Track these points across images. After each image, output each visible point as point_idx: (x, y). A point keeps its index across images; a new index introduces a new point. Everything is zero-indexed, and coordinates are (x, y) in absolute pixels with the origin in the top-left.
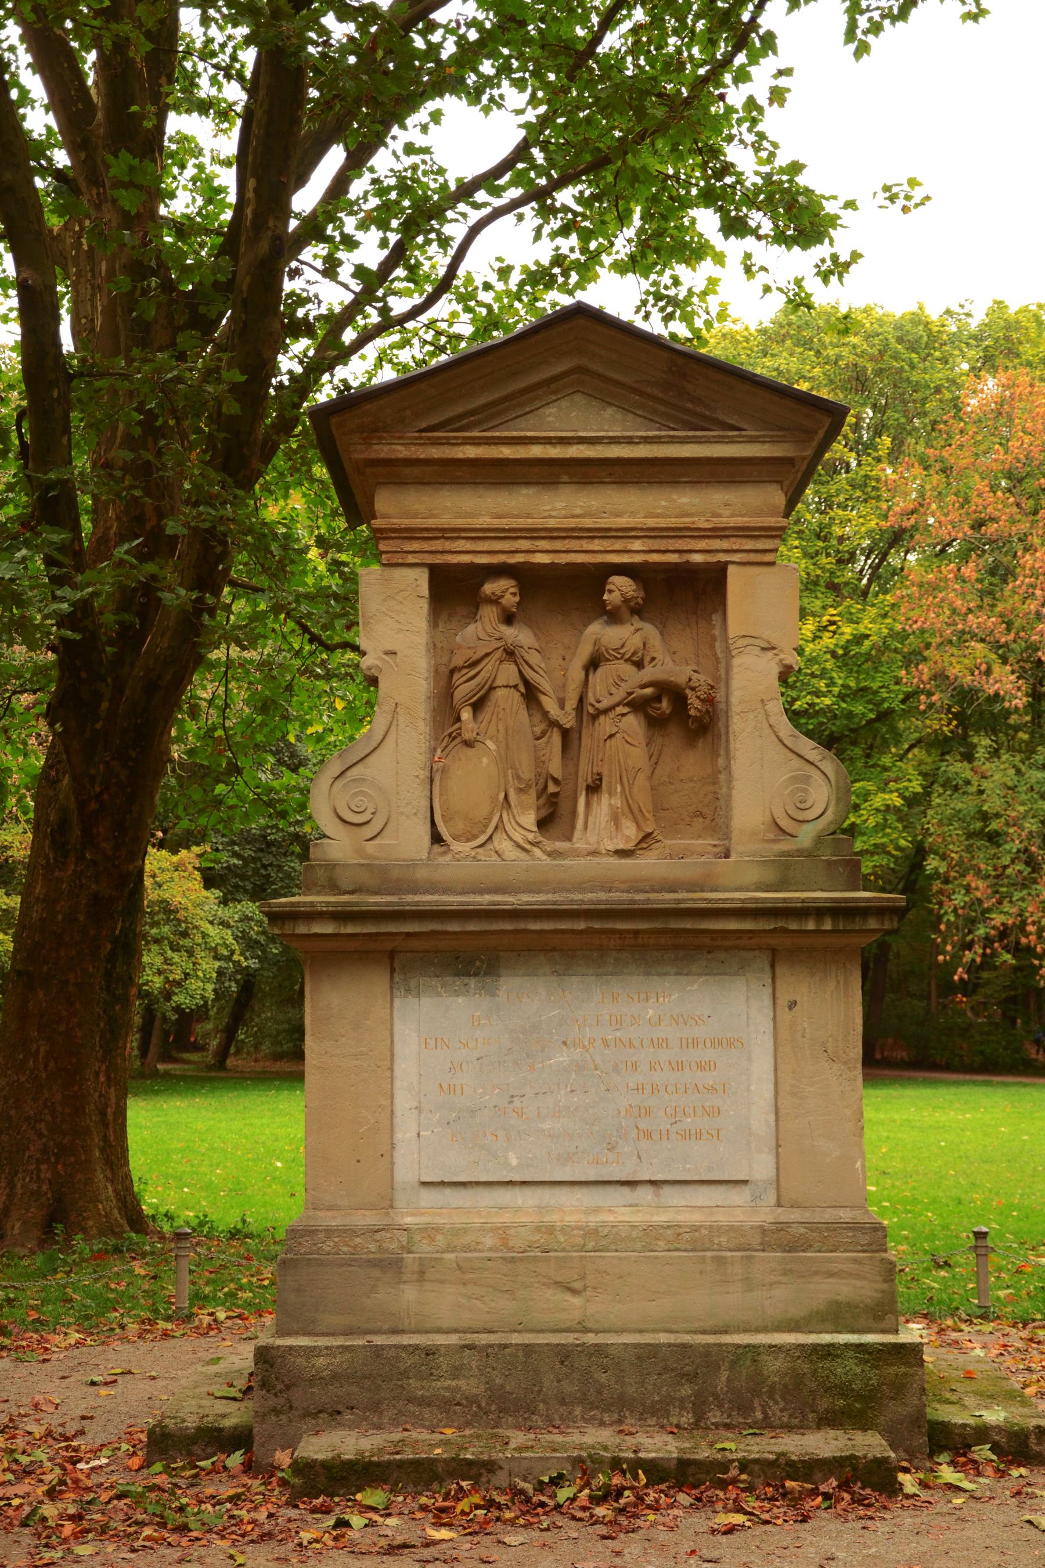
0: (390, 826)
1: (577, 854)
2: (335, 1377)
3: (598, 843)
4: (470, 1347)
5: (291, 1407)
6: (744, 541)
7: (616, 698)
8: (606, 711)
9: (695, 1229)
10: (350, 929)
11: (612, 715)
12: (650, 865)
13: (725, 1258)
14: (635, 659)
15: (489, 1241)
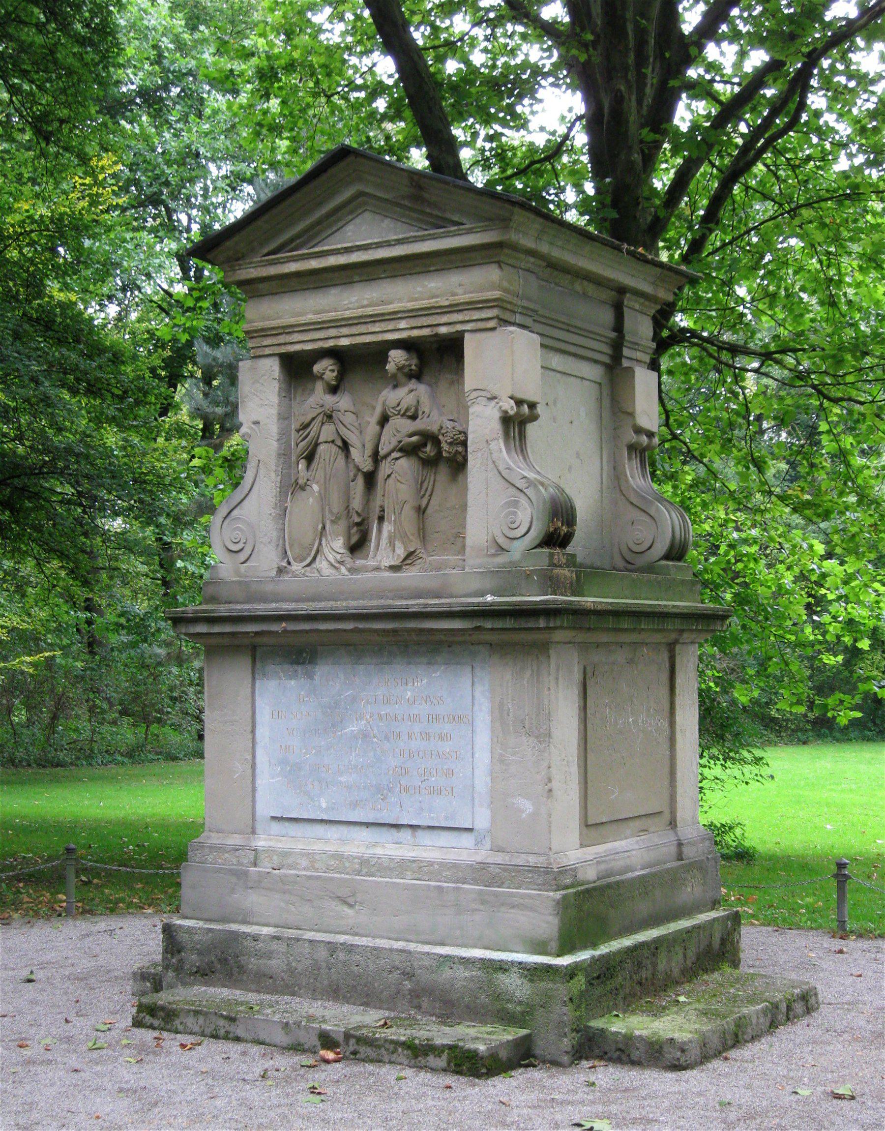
1: (365, 569)
4: (278, 938)
6: (473, 312)
7: (391, 447)
9: (431, 864)
11: (389, 459)
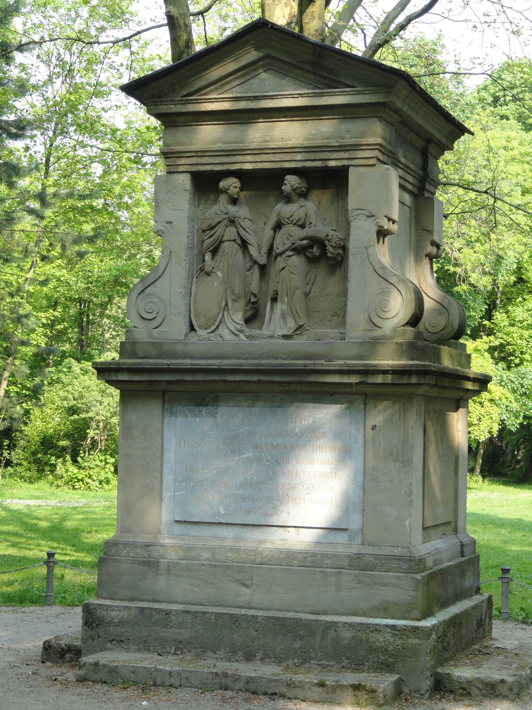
0: (166, 320)
1: (262, 337)
2: (122, 622)
3: (274, 331)
5: (99, 636)
7: (286, 247)
8: (281, 254)
10: (136, 378)
11: (284, 256)
12: (301, 343)
13: (326, 572)
14: (299, 223)
15: (206, 555)
